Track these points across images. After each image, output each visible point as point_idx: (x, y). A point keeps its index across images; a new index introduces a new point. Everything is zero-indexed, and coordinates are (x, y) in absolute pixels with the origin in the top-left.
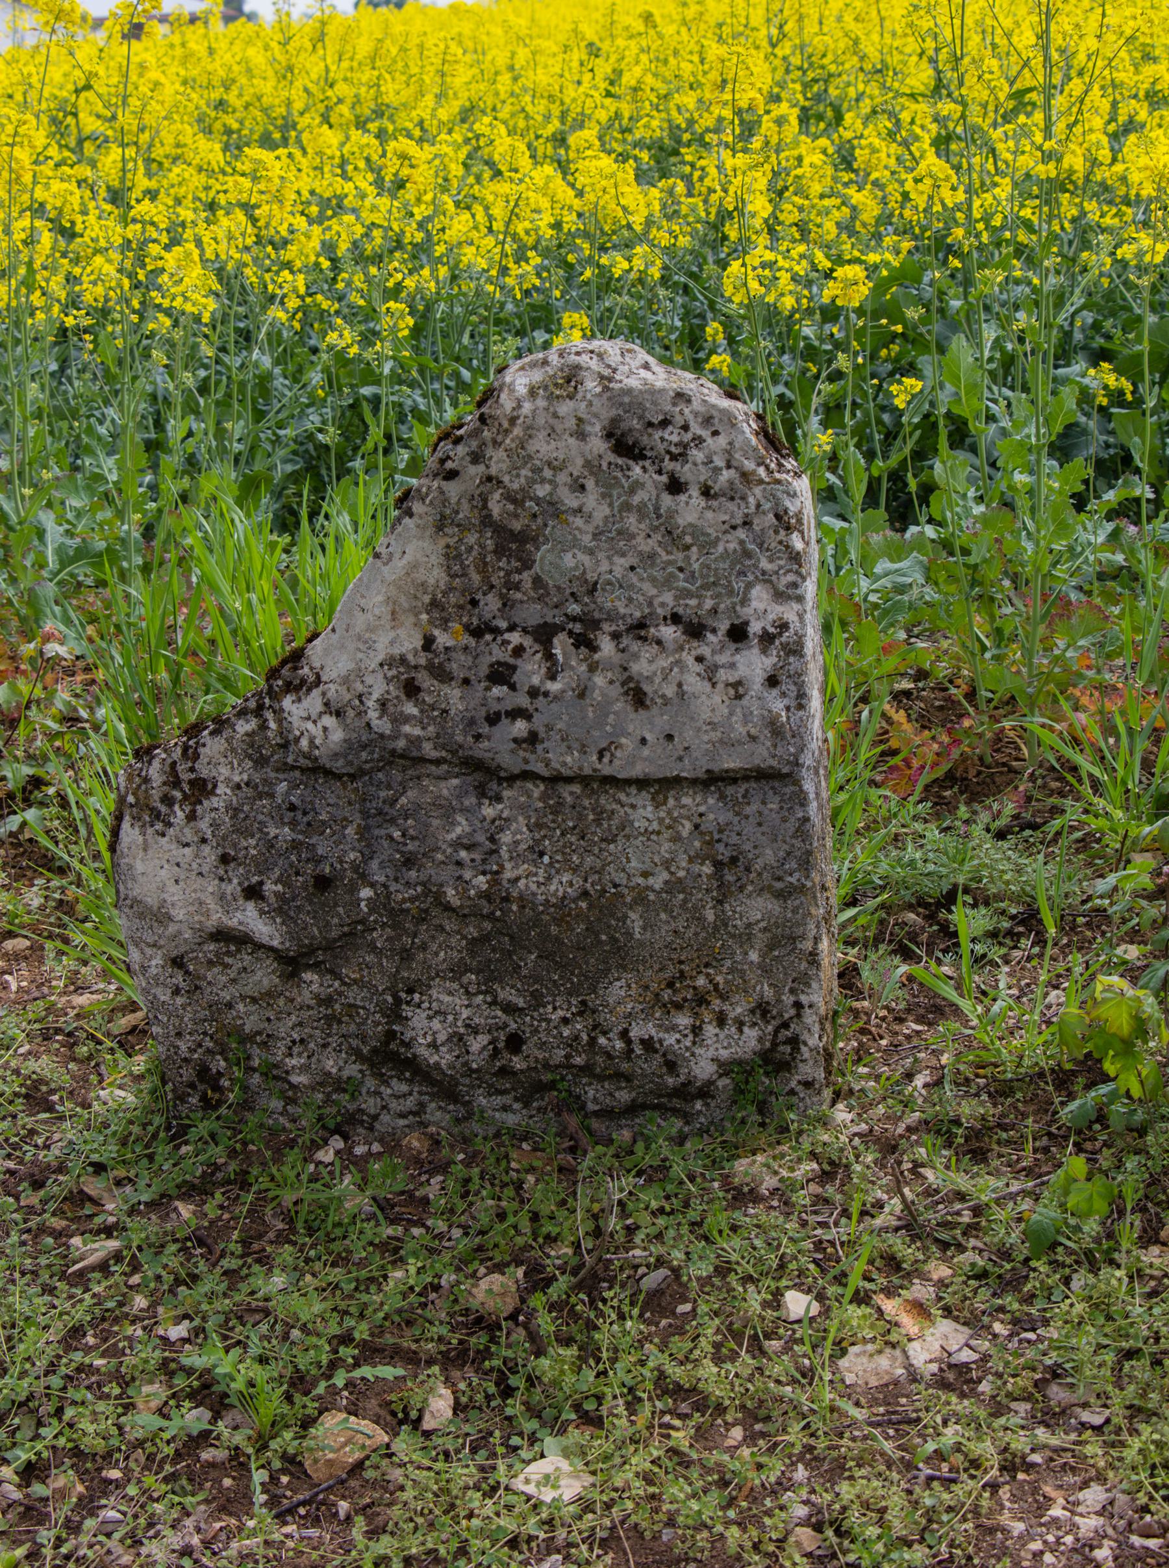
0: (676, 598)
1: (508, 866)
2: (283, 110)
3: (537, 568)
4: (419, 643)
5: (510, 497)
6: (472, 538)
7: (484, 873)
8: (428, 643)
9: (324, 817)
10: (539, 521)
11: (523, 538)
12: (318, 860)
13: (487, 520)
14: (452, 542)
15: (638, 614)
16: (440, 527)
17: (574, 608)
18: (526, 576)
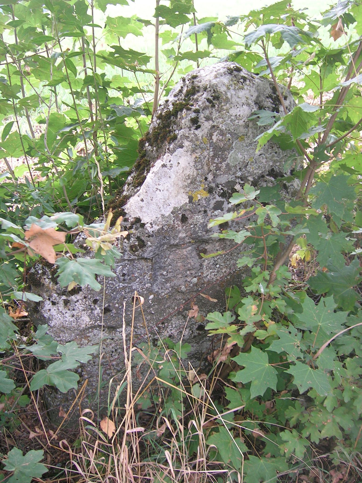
0: (273, 163)
2: (226, 69)
3: (228, 161)
4: (187, 201)
5: (222, 133)
6: (206, 153)
7: (195, 277)
8: (191, 199)
9: (136, 275)
10: (231, 141)
11: (223, 150)
13: (211, 144)
14: (197, 155)
15: (260, 172)
16: (193, 151)
17: (239, 174)
18: (224, 164)
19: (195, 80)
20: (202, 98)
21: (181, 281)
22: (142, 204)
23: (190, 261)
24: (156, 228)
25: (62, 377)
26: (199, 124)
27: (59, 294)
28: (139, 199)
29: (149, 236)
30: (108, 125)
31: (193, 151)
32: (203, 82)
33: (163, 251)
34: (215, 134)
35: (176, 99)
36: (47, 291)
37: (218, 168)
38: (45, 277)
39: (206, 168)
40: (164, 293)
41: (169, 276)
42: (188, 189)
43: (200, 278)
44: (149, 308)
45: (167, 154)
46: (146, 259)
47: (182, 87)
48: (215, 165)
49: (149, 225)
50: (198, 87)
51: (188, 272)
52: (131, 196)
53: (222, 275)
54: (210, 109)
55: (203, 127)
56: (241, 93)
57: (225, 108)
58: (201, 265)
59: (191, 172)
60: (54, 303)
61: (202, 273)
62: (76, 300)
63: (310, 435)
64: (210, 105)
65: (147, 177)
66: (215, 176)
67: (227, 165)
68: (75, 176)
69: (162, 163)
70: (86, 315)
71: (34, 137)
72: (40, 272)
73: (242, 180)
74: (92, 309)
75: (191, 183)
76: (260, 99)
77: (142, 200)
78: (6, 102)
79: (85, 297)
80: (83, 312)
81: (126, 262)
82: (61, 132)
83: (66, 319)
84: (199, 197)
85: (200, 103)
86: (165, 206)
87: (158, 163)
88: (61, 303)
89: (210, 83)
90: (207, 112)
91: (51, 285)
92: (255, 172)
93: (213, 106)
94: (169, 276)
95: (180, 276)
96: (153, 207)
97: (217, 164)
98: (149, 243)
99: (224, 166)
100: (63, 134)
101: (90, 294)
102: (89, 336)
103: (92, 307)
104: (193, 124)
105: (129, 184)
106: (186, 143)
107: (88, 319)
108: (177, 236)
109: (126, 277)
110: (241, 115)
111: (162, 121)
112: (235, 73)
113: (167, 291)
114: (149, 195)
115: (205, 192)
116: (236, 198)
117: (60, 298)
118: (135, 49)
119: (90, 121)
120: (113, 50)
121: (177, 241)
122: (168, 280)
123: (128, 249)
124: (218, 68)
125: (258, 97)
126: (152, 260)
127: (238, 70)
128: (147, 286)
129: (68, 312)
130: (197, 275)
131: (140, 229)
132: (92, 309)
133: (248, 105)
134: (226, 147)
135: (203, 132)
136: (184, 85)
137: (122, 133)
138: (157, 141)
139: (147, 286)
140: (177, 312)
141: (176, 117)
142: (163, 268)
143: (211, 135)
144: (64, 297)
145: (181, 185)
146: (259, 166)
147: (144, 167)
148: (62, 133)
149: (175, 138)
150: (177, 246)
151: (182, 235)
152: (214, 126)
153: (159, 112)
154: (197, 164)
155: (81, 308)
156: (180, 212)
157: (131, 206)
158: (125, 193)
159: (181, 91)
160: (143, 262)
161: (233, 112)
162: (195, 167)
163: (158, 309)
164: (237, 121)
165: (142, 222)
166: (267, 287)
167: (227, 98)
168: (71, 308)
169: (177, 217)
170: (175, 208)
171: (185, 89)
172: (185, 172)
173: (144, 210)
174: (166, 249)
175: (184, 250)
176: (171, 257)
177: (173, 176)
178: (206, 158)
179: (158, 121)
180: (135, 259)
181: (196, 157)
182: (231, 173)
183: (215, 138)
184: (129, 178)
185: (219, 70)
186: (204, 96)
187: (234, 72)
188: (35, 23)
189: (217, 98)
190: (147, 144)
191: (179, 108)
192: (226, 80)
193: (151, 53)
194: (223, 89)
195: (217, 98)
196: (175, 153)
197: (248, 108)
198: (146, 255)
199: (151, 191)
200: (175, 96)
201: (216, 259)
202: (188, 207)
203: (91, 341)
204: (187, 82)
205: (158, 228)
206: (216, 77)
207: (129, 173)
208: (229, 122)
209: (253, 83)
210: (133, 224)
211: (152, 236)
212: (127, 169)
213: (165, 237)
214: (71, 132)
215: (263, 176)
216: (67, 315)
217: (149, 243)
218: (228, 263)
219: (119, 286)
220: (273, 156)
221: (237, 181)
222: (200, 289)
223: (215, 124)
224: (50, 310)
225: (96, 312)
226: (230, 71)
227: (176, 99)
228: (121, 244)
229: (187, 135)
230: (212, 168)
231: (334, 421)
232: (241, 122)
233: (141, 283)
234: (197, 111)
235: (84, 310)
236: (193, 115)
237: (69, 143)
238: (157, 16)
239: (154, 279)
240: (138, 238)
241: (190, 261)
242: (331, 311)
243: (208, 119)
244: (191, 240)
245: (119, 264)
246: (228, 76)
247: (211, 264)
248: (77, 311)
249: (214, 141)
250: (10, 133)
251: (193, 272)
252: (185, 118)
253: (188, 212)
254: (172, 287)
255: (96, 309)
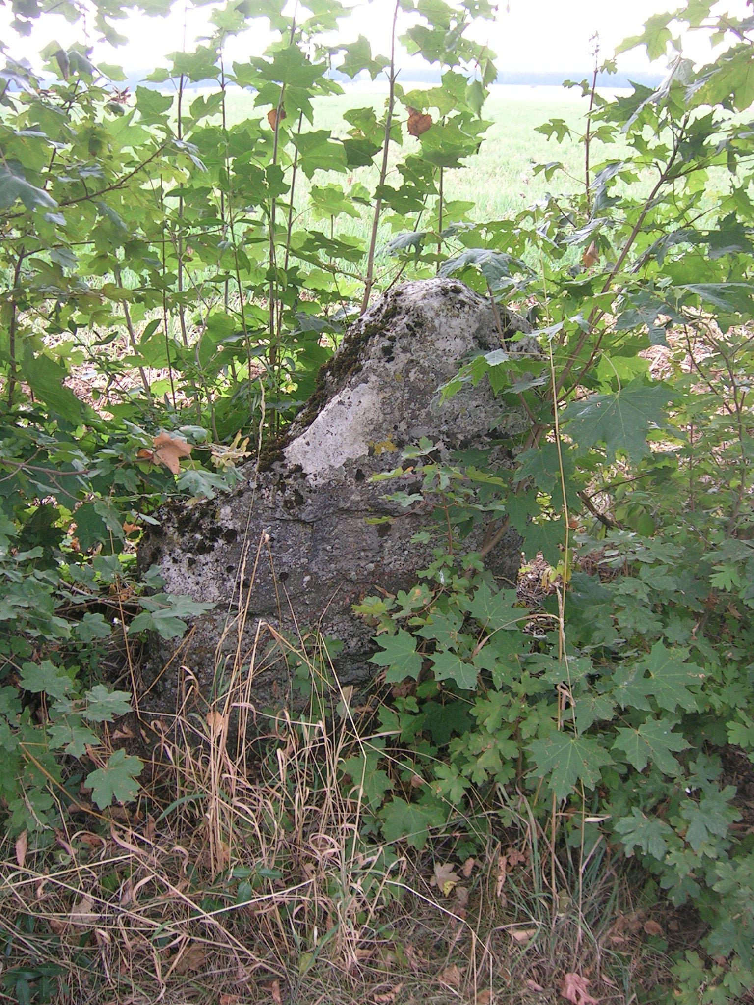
1: (386, 558)
3: (429, 408)
4: (367, 452)
5: (423, 371)
6: (398, 394)
7: (372, 562)
8: (371, 451)
9: (289, 543)
10: (435, 383)
11: (423, 393)
12: (282, 564)
13: (407, 383)
14: (387, 395)
15: (476, 430)
16: (381, 389)
17: (444, 428)
18: (423, 412)
19: (398, 298)
20: (402, 322)
21: (351, 565)
22: (307, 448)
23: (366, 537)
24: (321, 481)
25: (167, 624)
26: (393, 355)
27: (184, 551)
28: (304, 441)
29: (310, 491)
30: (295, 340)
31: (381, 389)
32: (407, 303)
33: (328, 516)
34: (414, 370)
35: (372, 319)
36: (169, 544)
37: (414, 417)
38: (170, 525)
39: (397, 413)
40: (325, 577)
41: (334, 553)
42: (369, 437)
43: (378, 564)
44: (303, 593)
45: (346, 389)
46: (304, 523)
47: (382, 305)
48: (410, 411)
49: (312, 476)
50: (400, 308)
51: (362, 554)
52: (296, 437)
53: (411, 568)
54: (409, 338)
55: (396, 360)
56: (455, 322)
57: (429, 338)
58: (381, 546)
59: (376, 415)
60: (175, 561)
61: (383, 558)
62: (204, 562)
63: (473, 773)
64: (410, 333)
65: (320, 415)
66: (410, 426)
67: (428, 414)
68: (235, 406)
69: (339, 399)
70: (214, 586)
71: (186, 343)
72: (164, 517)
73: (448, 437)
74: (224, 580)
75: (374, 430)
76: (482, 333)
77: (308, 444)
78: (154, 292)
79: (217, 561)
80: (212, 581)
81: (278, 522)
82: (225, 341)
83: (188, 586)
84: (383, 450)
85: (398, 329)
86: (336, 455)
87: (336, 399)
88: (186, 561)
89: (415, 305)
90: (405, 342)
91: (175, 537)
92: (468, 428)
93: (414, 335)
94: (334, 553)
95: (350, 557)
96: (321, 454)
97: (414, 411)
98: (310, 501)
99: (424, 414)
100: (227, 344)
101: (224, 557)
102: (215, 620)
103: (225, 576)
104: (385, 355)
105: (297, 422)
106: (373, 378)
107: (217, 593)
108: (348, 498)
109: (275, 543)
110: (452, 350)
111: (350, 346)
112: (451, 295)
113: (331, 575)
114: (317, 438)
115: (392, 445)
116: (408, 452)
117: (184, 555)
118: (629, 51)
119: (268, 331)
120: (313, 237)
121: (348, 505)
122: (332, 559)
123: (281, 504)
124: (430, 286)
125: (478, 329)
126: (312, 526)
127: (457, 291)
128: (302, 561)
129: (193, 576)
130: (375, 559)
131: (300, 480)
132: (224, 580)
133: (463, 338)
134: (428, 389)
135: (397, 367)
136: (385, 303)
137: (311, 354)
138: (339, 370)
139: (302, 561)
140: (341, 609)
141: (367, 342)
142: (328, 541)
143: (408, 372)
144: (190, 555)
145: (361, 431)
146: (474, 422)
147: (319, 402)
148: (229, 342)
149: (359, 369)
150: (347, 511)
151: (355, 497)
152: (412, 361)
153: (349, 333)
154: (386, 407)
155: (209, 574)
156: (355, 466)
157: (292, 449)
158: (290, 433)
159: (379, 310)
160: (300, 527)
161: (441, 345)
162: (382, 410)
163: (314, 598)
164: (445, 358)
165: (304, 471)
166: (450, 577)
167: (433, 326)
168: (197, 572)
169: (350, 471)
170: (348, 459)
171: (385, 308)
172: (366, 415)
173: (309, 456)
174: (333, 513)
175: (359, 520)
176: (339, 527)
177: (351, 418)
178: (399, 401)
179: (345, 346)
180: (290, 520)
181: (385, 398)
182: (433, 425)
183: (412, 376)
184: (300, 415)
185: (431, 288)
186: (405, 320)
187: (450, 293)
188: (212, 180)
189: (419, 325)
190: (329, 374)
191: (373, 331)
192: (436, 303)
193: (365, 247)
194: (430, 314)
195: (419, 325)
196: (357, 389)
197: (462, 342)
198: (303, 516)
199: (320, 433)
200: (371, 315)
201: (404, 542)
202: (366, 461)
203: (217, 627)
204: (389, 299)
205: (323, 482)
206: (424, 298)
207: (300, 409)
208: (434, 357)
209: (474, 311)
210: (292, 471)
211: (315, 492)
212: (301, 403)
213: (332, 497)
214: (240, 341)
215: (479, 436)
216: (190, 580)
217: (310, 501)
218: (422, 551)
219: (264, 553)
220: (496, 411)
221: (441, 437)
222: (377, 581)
223: (414, 358)
224: (169, 569)
225: (229, 584)
226: (445, 292)
227: (372, 319)
228: (274, 496)
229: (375, 367)
230: (406, 415)
231: (495, 746)
232: (451, 360)
233: (294, 555)
234: (392, 339)
235: (213, 578)
236: (387, 343)
237: (235, 358)
238: (377, 197)
239: (312, 554)
240: (296, 491)
241: (366, 537)
242: (508, 605)
243: (405, 350)
244: (368, 507)
245: (268, 524)
246: (441, 299)
247: (396, 547)
248: (204, 578)
249: (412, 380)
250: (155, 333)
251: (370, 554)
252: (377, 344)
253: (367, 468)
254: (338, 570)
255: (229, 580)
